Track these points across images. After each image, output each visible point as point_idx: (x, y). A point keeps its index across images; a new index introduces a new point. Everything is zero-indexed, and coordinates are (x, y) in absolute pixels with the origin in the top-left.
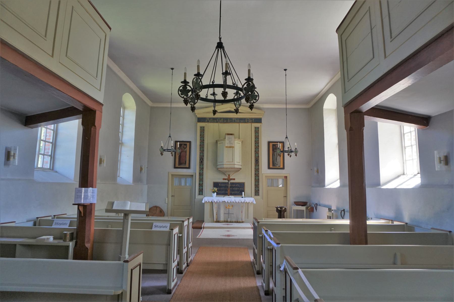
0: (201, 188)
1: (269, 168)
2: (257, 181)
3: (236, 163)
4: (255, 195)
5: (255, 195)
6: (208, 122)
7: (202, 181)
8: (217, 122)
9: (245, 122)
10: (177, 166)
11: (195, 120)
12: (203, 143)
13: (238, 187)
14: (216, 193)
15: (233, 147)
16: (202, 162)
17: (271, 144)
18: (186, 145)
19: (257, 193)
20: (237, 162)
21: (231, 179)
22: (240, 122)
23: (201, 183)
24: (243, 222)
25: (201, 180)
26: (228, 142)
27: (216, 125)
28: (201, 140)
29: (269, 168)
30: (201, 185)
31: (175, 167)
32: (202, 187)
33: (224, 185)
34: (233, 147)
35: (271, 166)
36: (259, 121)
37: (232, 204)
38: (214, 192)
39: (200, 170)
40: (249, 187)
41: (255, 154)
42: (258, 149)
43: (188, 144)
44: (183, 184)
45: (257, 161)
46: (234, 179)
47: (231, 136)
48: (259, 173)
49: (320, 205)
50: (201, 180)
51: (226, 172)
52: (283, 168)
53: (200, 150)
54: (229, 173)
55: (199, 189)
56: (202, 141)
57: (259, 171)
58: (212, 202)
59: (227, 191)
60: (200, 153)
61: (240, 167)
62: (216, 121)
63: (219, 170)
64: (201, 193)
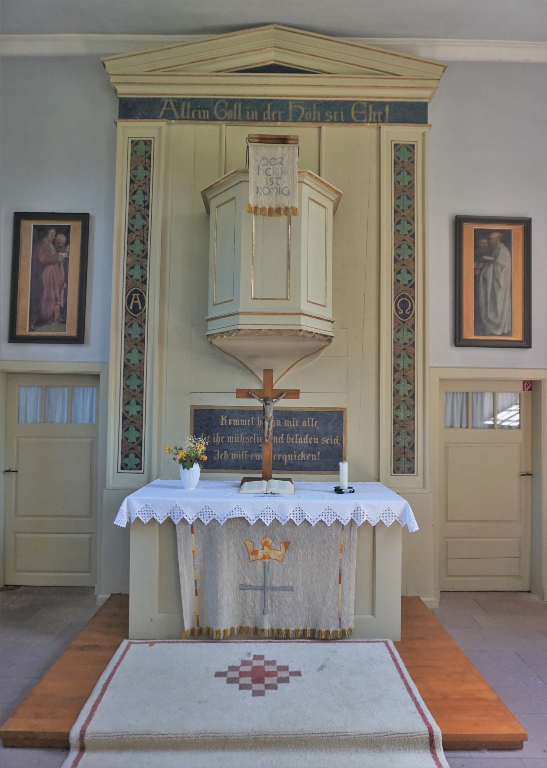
0: (133, 435)
1: (458, 340)
2: (405, 402)
3: (305, 307)
4: (397, 470)
5: (397, 470)
6: (169, 116)
7: (139, 403)
8: (213, 119)
9: (348, 121)
10: (24, 329)
11: (111, 109)
12: (145, 217)
13: (313, 433)
14: (196, 467)
15: (289, 212)
16: (136, 309)
17: (469, 230)
18: (66, 231)
19: (404, 459)
20: (313, 304)
21: (280, 394)
22: (323, 120)
23: (133, 410)
24: (342, 636)
25: (133, 396)
26: (262, 182)
27: (208, 130)
28: (132, 202)
29: (458, 340)
30: (132, 422)
31: (14, 338)
32: (139, 429)
33: (244, 422)
34: (289, 212)
35: (469, 333)
36: (414, 113)
37: (286, 535)
38: (187, 462)
39: (128, 351)
40: (365, 437)
41: (398, 272)
42: (411, 247)
43: (76, 226)
44: (59, 414)
45: (404, 305)
46: (294, 394)
47: (279, 147)
48: (412, 367)
49: (532, 478)
50: (133, 396)
51: (254, 357)
52: (526, 343)
53: (130, 253)
54: (268, 364)
55: (125, 440)
56: (140, 210)
57: (412, 356)
58: (169, 521)
59: (260, 451)
60: (130, 267)
61: (324, 328)
62: (206, 113)
63: (218, 347)
64: (132, 460)
